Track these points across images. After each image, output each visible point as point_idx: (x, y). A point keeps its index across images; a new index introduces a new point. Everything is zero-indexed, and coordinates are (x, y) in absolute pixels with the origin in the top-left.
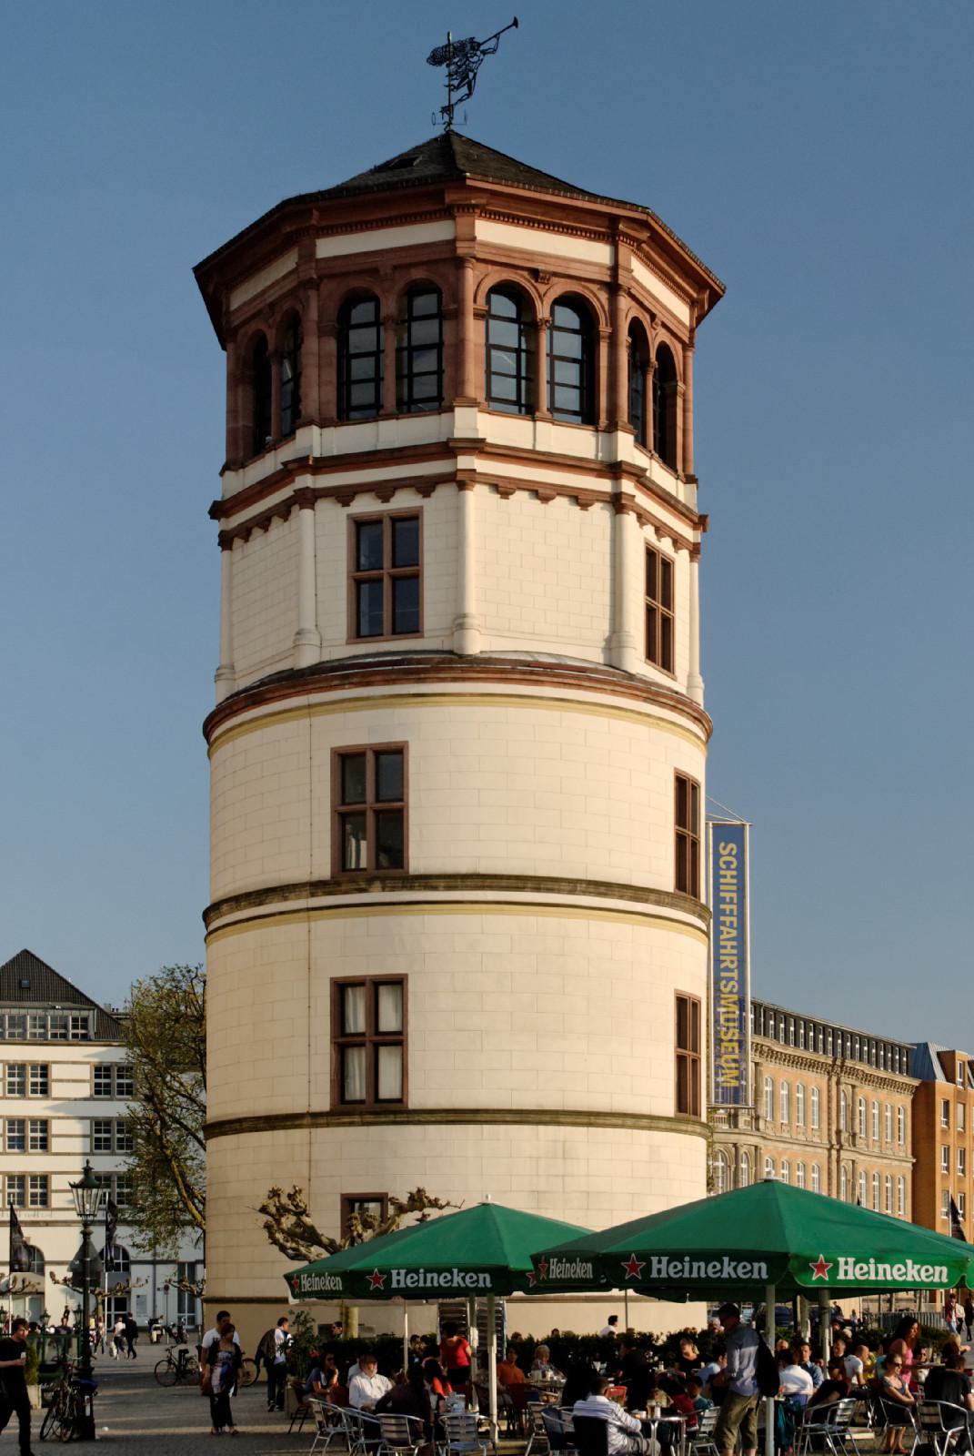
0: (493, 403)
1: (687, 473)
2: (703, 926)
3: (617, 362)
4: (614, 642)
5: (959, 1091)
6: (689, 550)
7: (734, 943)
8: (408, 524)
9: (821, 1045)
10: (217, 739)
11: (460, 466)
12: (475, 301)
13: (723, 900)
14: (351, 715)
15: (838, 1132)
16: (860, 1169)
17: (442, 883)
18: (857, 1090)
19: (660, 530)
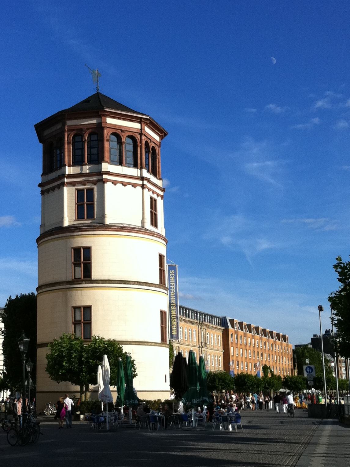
0: (112, 162)
1: (160, 178)
2: (167, 293)
3: (142, 152)
4: (143, 222)
5: (236, 331)
7: (174, 296)
8: (91, 191)
9: (196, 317)
10: (40, 244)
11: (104, 178)
12: (107, 137)
13: (171, 285)
15: (202, 343)
16: (208, 353)
17: (101, 282)
18: (206, 330)
19: (154, 192)
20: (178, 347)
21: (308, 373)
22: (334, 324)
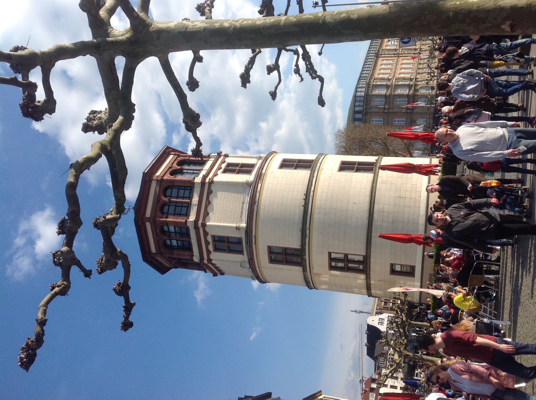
0: (187, 215)
14: (260, 253)
15: (394, 54)
20: (396, 79)
21: (410, 40)
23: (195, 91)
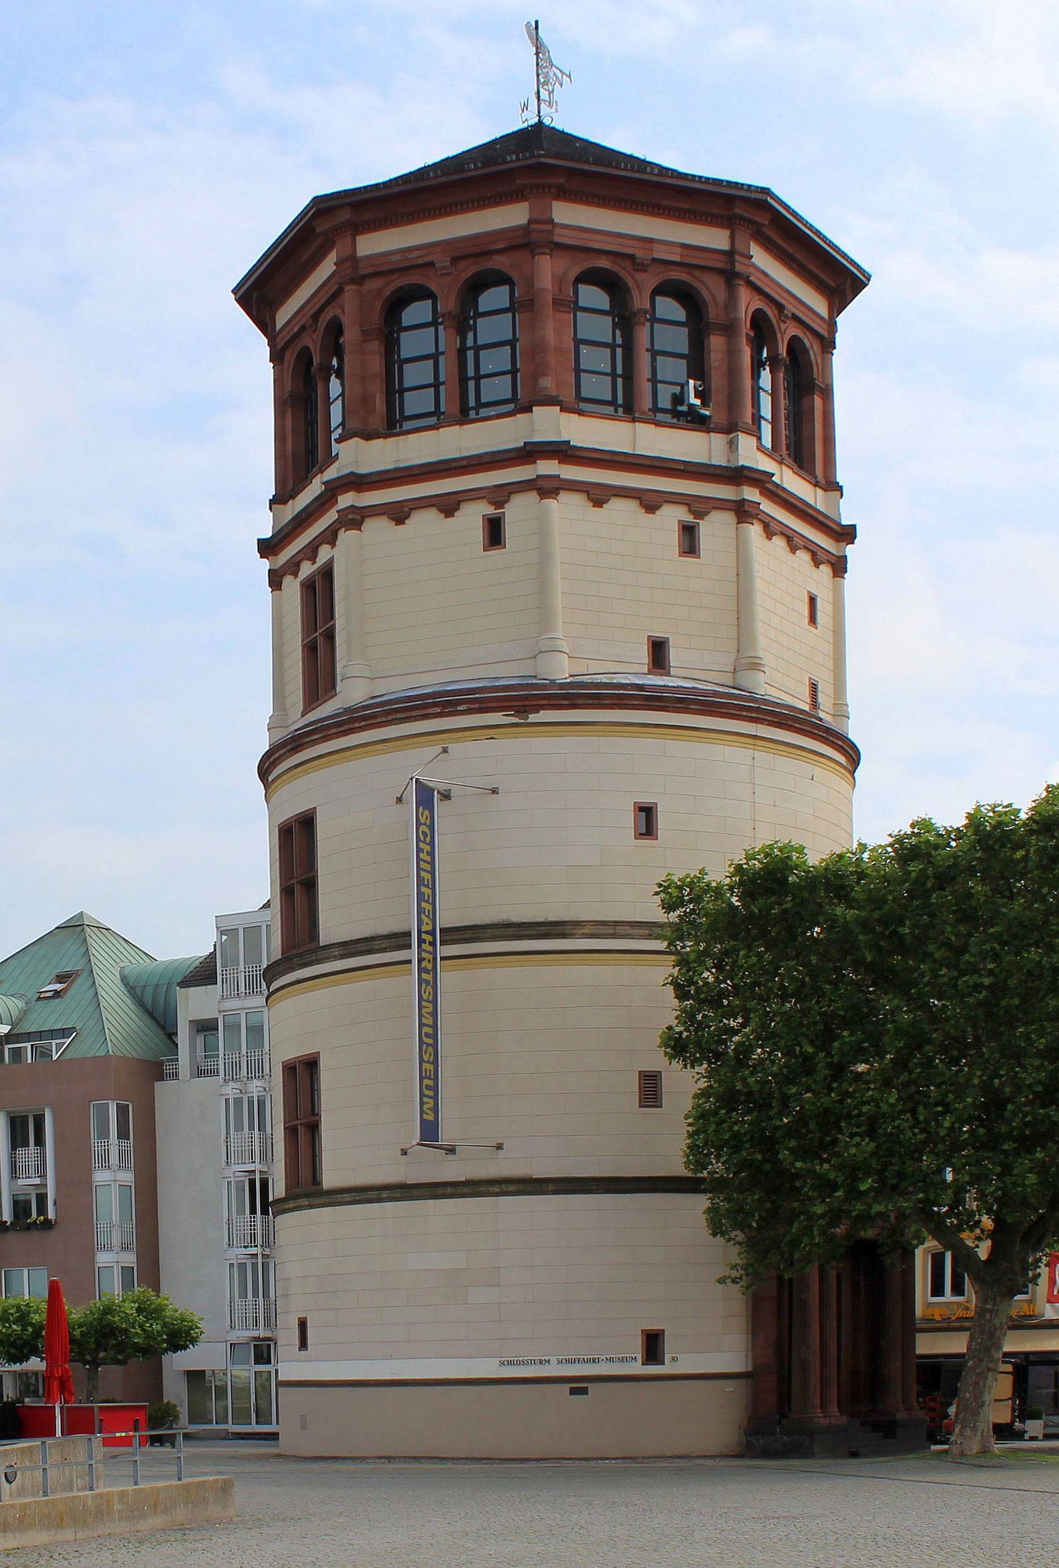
6: (847, 544)
22: (1029, 1061)
23: (404, 523)
